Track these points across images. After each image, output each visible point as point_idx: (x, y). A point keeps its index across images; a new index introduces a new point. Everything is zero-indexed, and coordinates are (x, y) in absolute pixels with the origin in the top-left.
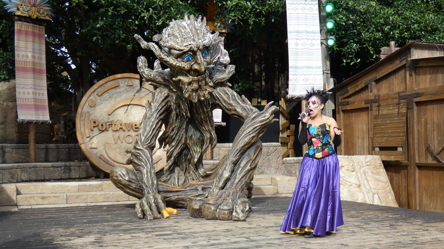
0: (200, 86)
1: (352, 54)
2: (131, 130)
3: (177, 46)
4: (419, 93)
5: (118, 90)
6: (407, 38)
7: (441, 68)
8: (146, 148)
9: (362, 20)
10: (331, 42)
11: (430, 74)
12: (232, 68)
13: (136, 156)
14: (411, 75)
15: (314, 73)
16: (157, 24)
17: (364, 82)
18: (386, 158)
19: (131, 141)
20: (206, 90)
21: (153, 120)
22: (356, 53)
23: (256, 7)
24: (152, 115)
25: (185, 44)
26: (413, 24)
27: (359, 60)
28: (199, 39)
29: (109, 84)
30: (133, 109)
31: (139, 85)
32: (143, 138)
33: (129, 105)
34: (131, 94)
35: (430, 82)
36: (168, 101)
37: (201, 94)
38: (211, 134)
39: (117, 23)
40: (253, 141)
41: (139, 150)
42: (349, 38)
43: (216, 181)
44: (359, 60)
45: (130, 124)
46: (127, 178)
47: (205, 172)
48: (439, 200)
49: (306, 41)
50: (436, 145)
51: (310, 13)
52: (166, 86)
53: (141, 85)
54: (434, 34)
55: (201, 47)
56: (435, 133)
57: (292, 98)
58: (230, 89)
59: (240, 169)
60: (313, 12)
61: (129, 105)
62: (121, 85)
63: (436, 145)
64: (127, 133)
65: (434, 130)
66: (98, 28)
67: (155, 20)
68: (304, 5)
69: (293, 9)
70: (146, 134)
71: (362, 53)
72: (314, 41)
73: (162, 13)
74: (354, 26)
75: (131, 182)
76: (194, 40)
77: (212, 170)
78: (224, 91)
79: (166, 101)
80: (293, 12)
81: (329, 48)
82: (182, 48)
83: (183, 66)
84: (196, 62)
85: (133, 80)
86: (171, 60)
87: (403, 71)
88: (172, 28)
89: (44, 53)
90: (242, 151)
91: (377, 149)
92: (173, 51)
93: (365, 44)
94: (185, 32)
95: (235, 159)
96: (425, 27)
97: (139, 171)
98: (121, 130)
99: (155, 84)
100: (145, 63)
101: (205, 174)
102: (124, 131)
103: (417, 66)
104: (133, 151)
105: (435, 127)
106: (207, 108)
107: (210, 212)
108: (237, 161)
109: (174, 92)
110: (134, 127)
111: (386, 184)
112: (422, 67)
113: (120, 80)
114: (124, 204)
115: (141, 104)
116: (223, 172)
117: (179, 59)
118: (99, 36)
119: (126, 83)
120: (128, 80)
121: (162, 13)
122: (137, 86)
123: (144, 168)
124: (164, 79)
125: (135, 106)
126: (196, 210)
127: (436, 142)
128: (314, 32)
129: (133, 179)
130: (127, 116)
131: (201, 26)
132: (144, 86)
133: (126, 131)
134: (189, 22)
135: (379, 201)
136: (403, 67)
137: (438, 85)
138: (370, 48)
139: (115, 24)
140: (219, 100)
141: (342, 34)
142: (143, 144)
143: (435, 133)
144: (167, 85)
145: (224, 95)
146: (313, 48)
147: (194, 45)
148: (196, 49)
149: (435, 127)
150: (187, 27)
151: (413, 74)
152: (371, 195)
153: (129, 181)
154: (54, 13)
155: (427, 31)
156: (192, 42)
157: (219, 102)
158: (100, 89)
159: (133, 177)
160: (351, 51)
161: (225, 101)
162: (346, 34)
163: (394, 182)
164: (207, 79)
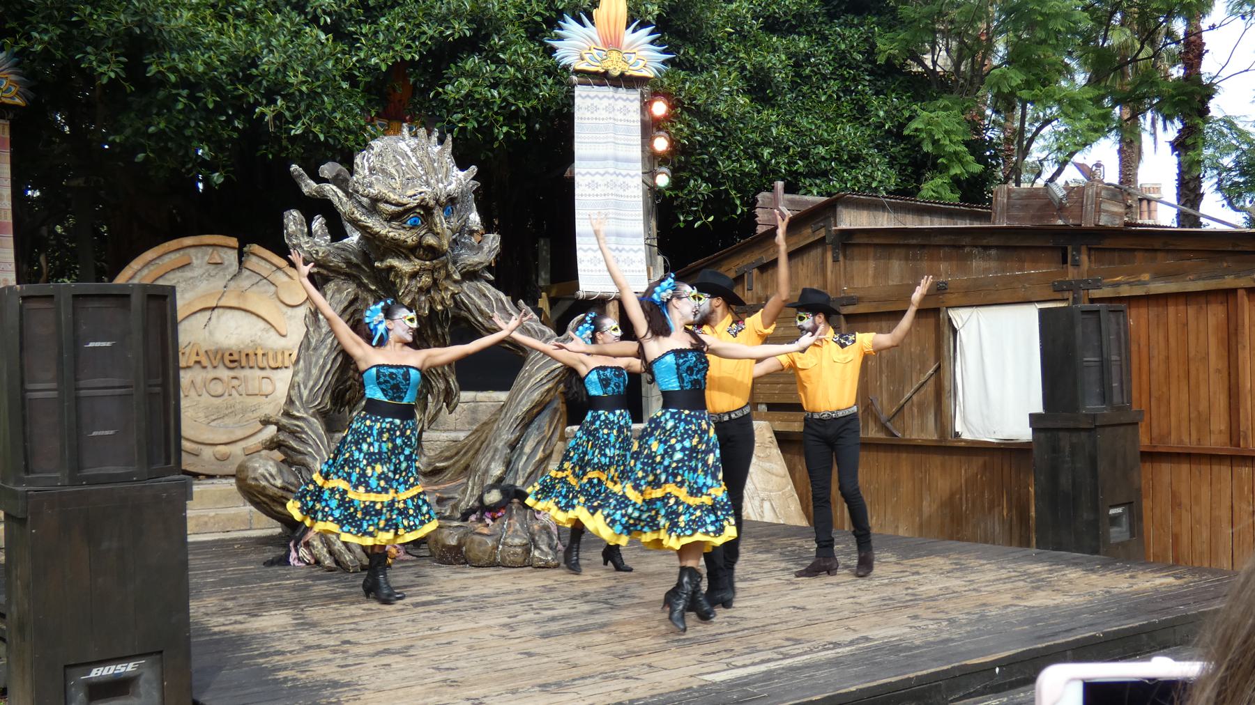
0: (435, 281)
1: (697, 205)
2: (221, 365)
3: (393, 197)
4: (852, 298)
5: (188, 274)
6: (801, 174)
7: (897, 250)
8: (314, 415)
9: (720, 134)
10: (663, 180)
11: (875, 259)
12: (493, 242)
13: (293, 433)
14: (835, 260)
15: (627, 248)
16: (293, 133)
17: (735, 269)
18: (781, 427)
19: (220, 391)
20: (446, 289)
21: (325, 352)
22: (705, 201)
23: (511, 100)
24: (323, 341)
25: (410, 193)
26: (815, 144)
27: (711, 219)
28: (438, 182)
29: (166, 259)
30: (223, 318)
31: (236, 263)
32: (305, 393)
33: (213, 309)
34: (218, 283)
35: (875, 277)
36: (356, 311)
37: (437, 297)
38: (448, 382)
39: (192, 124)
40: (548, 399)
41: (298, 418)
42: (691, 171)
43: (474, 484)
44: (711, 219)
45: (217, 352)
46: (279, 483)
47: (430, 464)
48: (889, 510)
49: (614, 177)
50: (885, 403)
51: (623, 117)
52: (349, 277)
53: (240, 262)
54: (853, 168)
55: (443, 199)
56: (884, 379)
57: (588, 297)
58: (489, 286)
59: (525, 458)
60: (628, 117)
61: (213, 309)
62: (195, 262)
63: (885, 403)
64: (211, 374)
65: (881, 372)
66: (152, 135)
67: (288, 122)
68: (612, 101)
69: (587, 109)
70: (311, 383)
71: (719, 203)
72: (628, 179)
73: (303, 107)
74: (704, 146)
75: (288, 490)
76: (428, 184)
77: (447, 459)
78: (479, 290)
79: (351, 310)
80: (588, 115)
81: (653, 193)
82: (405, 200)
83: (403, 237)
84: (430, 231)
85: (222, 252)
86: (377, 226)
87: (819, 250)
88: (380, 155)
89: (8, 183)
90: (526, 420)
91: (763, 408)
92: (382, 206)
93: (724, 184)
94: (407, 165)
95: (513, 437)
96: (837, 152)
97: (304, 465)
98: (198, 366)
99: (325, 272)
100: (302, 225)
101: (430, 469)
102: (205, 367)
103: (849, 241)
104: (284, 421)
105: (884, 366)
106: (442, 327)
107: (485, 552)
108: (517, 440)
109: (371, 290)
110: (227, 358)
111: (784, 480)
112: (859, 245)
113: (192, 251)
114: (245, 538)
115: (242, 306)
116: (489, 465)
117: (394, 224)
118: (152, 151)
119: (207, 258)
120: (210, 250)
121: (303, 107)
122: (231, 265)
123: (315, 459)
124: (349, 263)
125: (228, 311)
126: (450, 548)
127: (885, 396)
128: (628, 160)
129: (292, 484)
130: (210, 333)
131: (441, 153)
132: (248, 265)
133: (209, 366)
134: (413, 142)
135: (772, 514)
136: (821, 242)
137: (891, 283)
138: (733, 193)
139: (187, 125)
140: (469, 310)
141: (680, 161)
142: (305, 405)
143: (884, 379)
144: (354, 276)
145: (479, 298)
146: (626, 193)
147: (427, 193)
148: (432, 203)
149: (884, 366)
150: (410, 154)
151: (841, 258)
152: (757, 503)
153: (283, 488)
154: (31, 89)
155: (840, 161)
156: (424, 189)
157: (466, 314)
158: (145, 272)
159: (293, 480)
160: (696, 198)
161: (481, 312)
162: (687, 162)
163: (797, 475)
164: (450, 266)
